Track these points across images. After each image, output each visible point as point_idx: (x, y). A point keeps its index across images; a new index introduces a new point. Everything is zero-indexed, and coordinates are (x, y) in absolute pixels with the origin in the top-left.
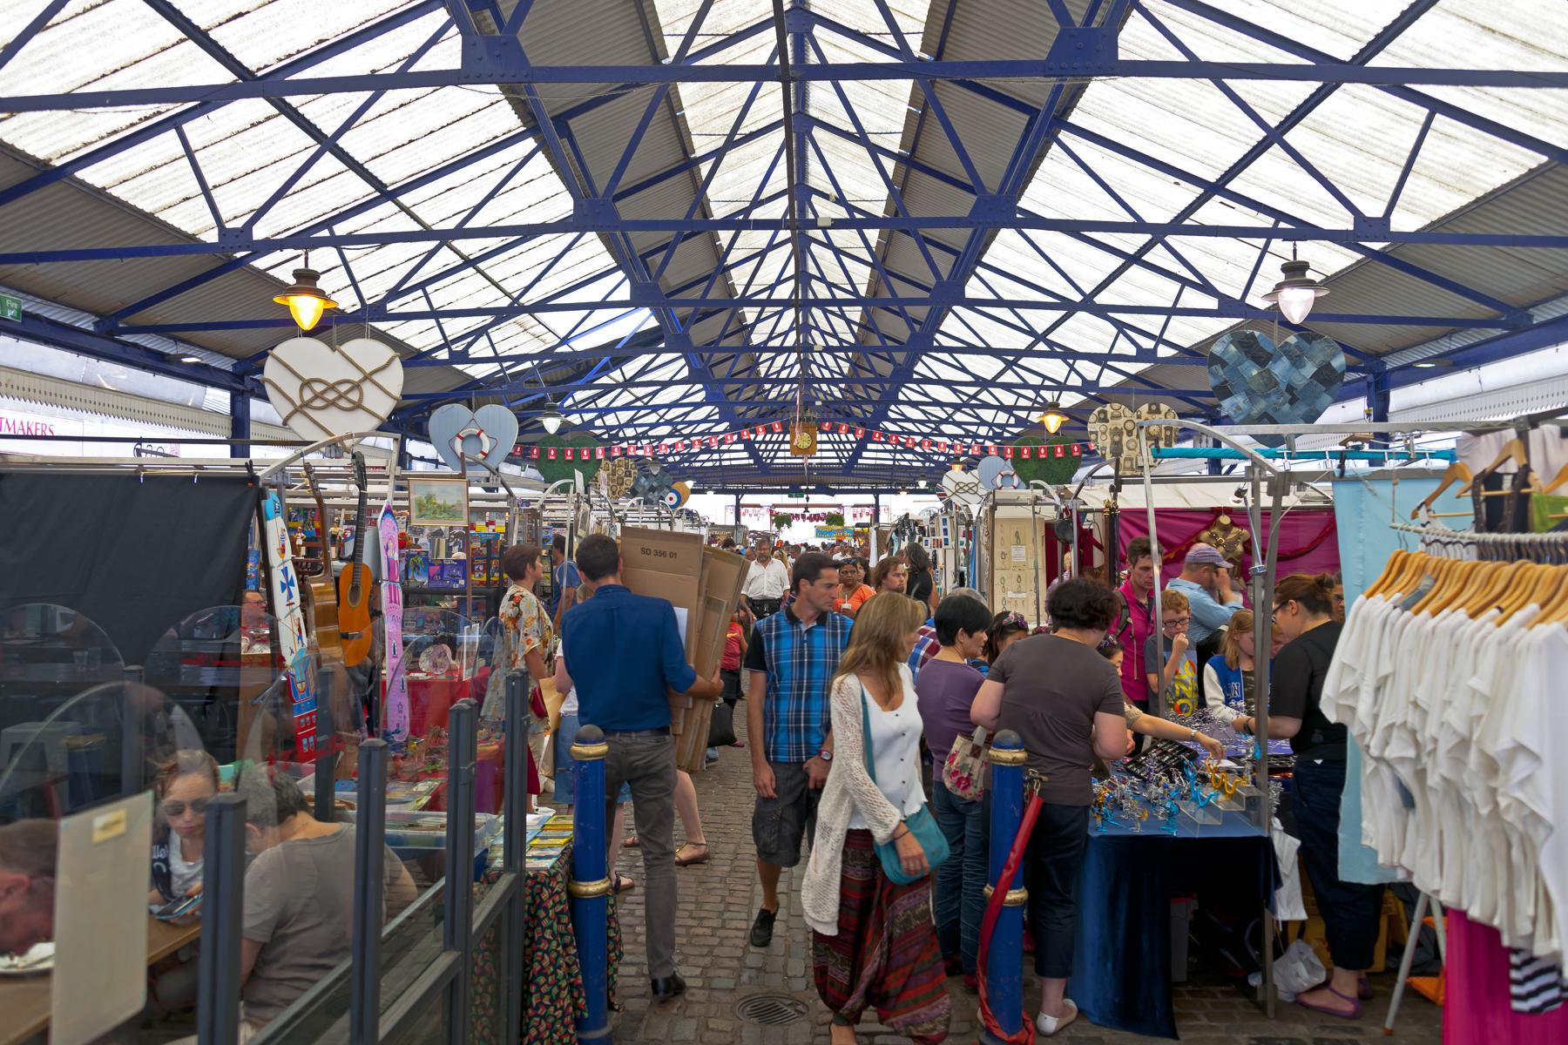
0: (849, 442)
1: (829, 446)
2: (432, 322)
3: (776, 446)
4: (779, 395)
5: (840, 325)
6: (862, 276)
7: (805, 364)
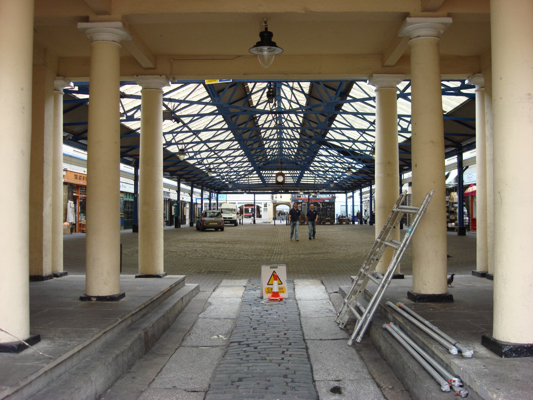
0: (297, 173)
1: (290, 175)
2: (176, 146)
3: (269, 178)
4: (272, 153)
5: (290, 152)
6: (303, 101)
7: (280, 144)
